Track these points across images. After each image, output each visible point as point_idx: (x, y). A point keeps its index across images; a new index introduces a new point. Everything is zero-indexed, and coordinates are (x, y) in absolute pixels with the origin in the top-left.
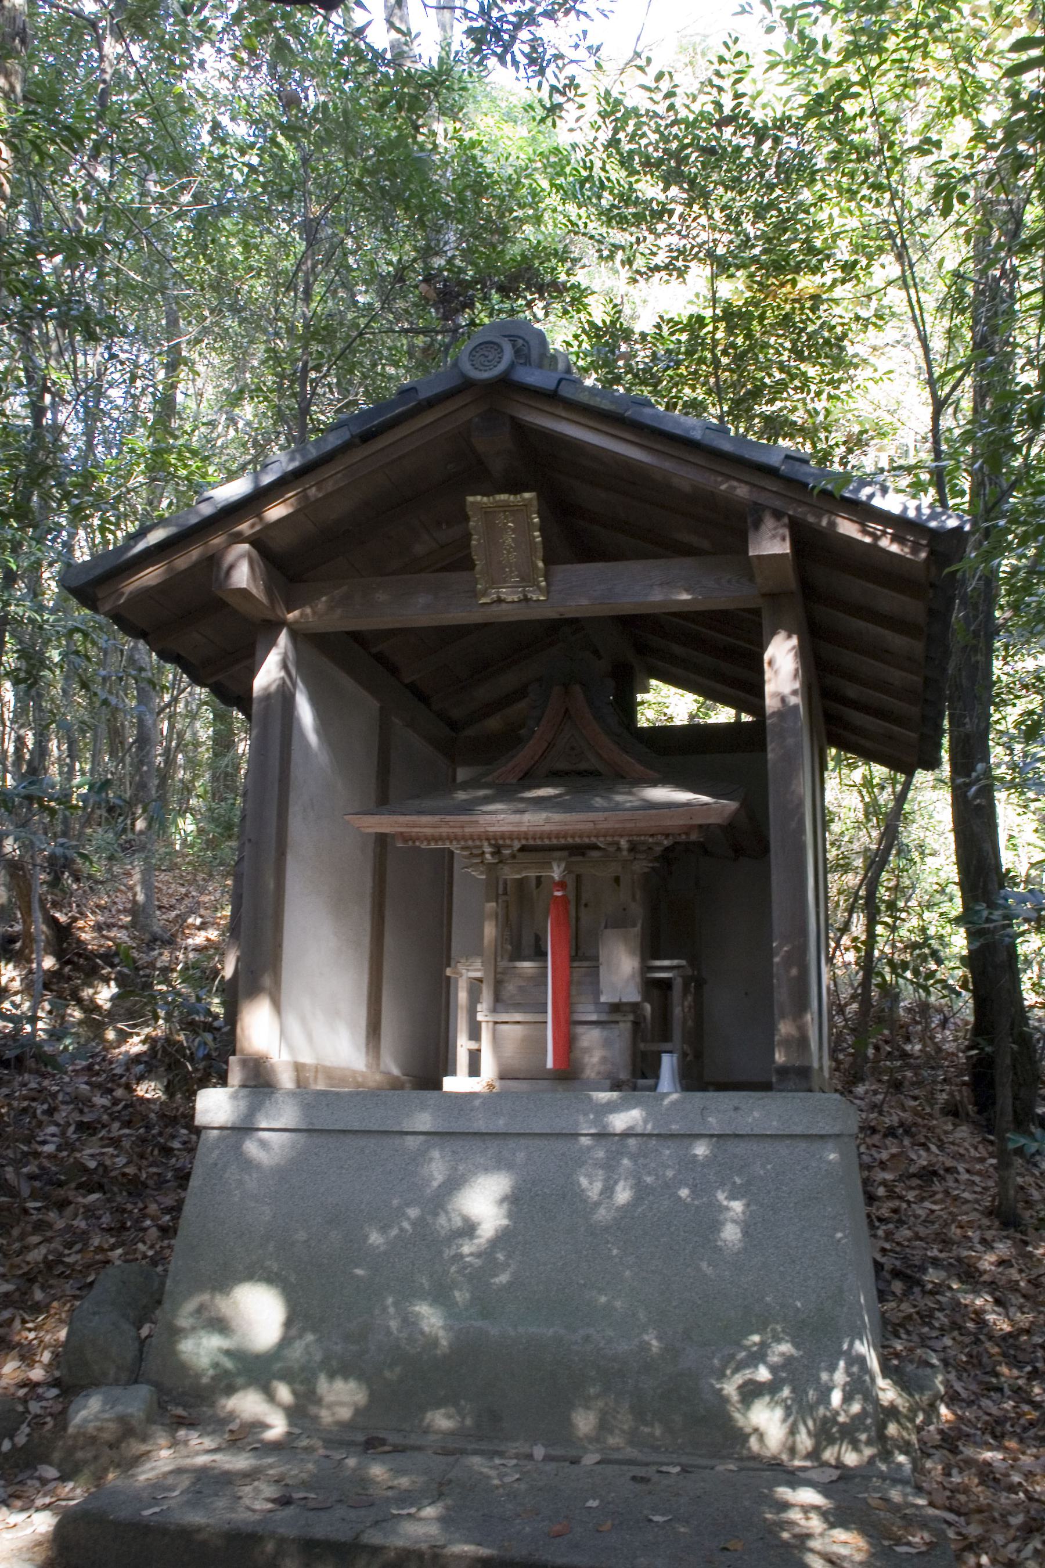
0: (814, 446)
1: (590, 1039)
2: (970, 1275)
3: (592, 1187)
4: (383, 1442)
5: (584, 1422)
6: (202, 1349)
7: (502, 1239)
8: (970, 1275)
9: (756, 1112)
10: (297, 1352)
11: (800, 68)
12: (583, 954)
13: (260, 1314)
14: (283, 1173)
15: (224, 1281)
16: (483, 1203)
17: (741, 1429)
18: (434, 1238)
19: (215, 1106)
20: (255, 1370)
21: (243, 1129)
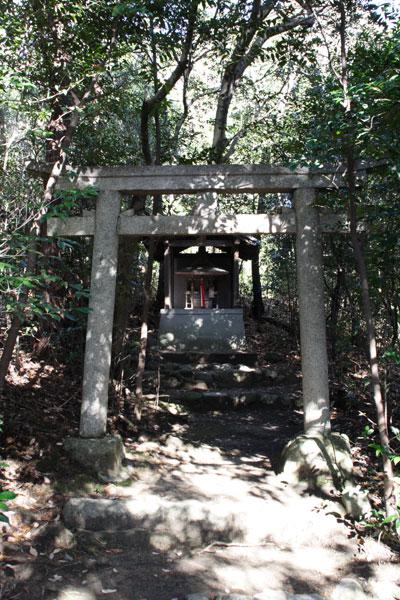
0: (368, 322)
1: (207, 302)
2: (254, 338)
3: (213, 319)
4: (99, 438)
5: (213, 347)
6: (163, 341)
7: (203, 326)
8: (254, 338)
9: (233, 311)
10: (176, 341)
11: (349, 522)
12: (207, 291)
13: (171, 337)
14: (173, 319)
15: (166, 332)
16: (199, 322)
17: (66, 588)
18: (193, 327)
19: (163, 311)
20: (171, 343)
21: (167, 314)
